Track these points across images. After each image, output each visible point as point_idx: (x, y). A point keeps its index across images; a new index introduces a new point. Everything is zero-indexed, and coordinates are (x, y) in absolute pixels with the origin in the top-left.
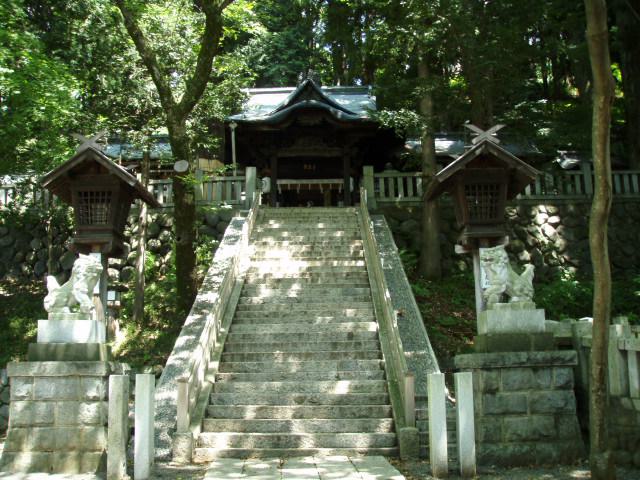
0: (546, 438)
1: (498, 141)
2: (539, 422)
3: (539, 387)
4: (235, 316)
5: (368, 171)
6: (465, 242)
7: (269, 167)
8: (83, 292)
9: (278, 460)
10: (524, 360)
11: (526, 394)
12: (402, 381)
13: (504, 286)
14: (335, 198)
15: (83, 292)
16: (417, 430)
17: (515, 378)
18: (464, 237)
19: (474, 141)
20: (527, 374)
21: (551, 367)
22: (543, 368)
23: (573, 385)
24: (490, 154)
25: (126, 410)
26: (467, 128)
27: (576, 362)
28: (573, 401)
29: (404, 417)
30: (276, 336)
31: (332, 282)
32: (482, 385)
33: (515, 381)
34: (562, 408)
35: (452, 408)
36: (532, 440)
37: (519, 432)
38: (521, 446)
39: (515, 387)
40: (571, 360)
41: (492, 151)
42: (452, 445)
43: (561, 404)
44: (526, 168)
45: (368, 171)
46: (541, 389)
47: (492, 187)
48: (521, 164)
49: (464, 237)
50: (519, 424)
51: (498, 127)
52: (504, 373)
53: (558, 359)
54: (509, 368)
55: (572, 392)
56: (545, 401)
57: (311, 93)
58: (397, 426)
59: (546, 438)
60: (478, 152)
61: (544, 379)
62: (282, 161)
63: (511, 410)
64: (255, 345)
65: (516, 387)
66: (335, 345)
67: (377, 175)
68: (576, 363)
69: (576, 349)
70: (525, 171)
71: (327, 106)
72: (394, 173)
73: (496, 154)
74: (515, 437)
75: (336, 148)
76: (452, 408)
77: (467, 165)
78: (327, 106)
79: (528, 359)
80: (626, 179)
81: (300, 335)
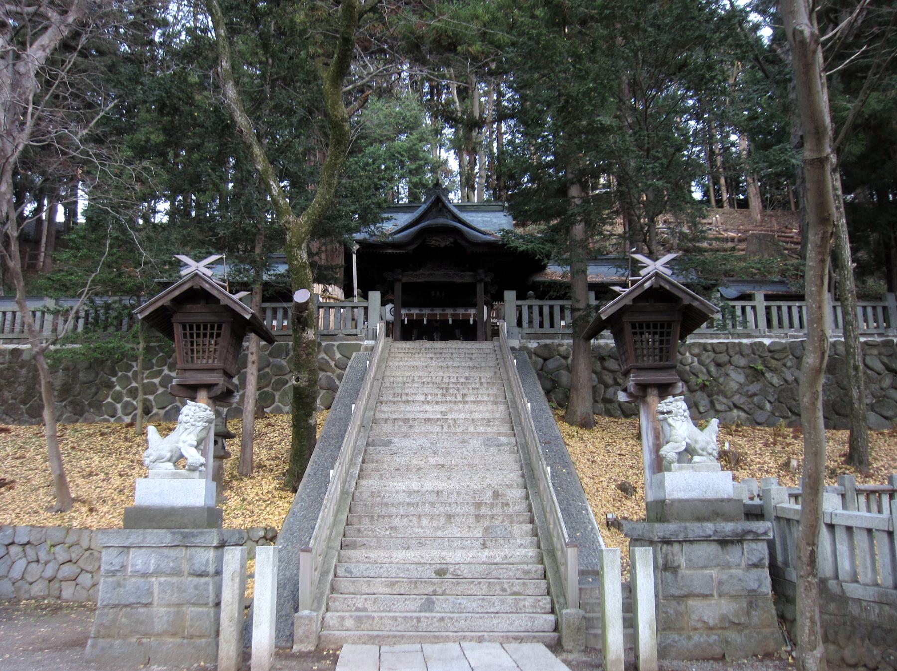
0: (737, 626)
1: (669, 272)
2: (727, 607)
3: (728, 566)
4: (361, 470)
5: (510, 296)
6: (632, 389)
7: (393, 293)
8: (191, 446)
9: (50, 303)
10: (711, 533)
11: (714, 572)
12: (564, 554)
13: (684, 444)
14: (467, 331)
15: (191, 446)
16: (581, 612)
17: (700, 553)
18: (631, 382)
19: (643, 272)
20: (713, 549)
21: (740, 542)
22: (732, 542)
23: (767, 562)
24: (661, 287)
25: (243, 588)
26: (633, 258)
27: (771, 535)
28: (768, 582)
29: (564, 596)
30: (410, 493)
31: (471, 429)
32: (661, 562)
33: (699, 557)
34: (755, 591)
35: (629, 590)
36: (721, 628)
37: (705, 619)
38: (708, 636)
39: (700, 565)
40: (766, 533)
41: (663, 284)
42: (631, 631)
43: (755, 586)
44: (702, 303)
45: (510, 296)
46: (730, 568)
47: (662, 327)
48: (697, 300)
49: (631, 382)
50: (708, 611)
51: (669, 257)
52: (686, 547)
53: (750, 531)
54: (691, 542)
55: (767, 572)
56: (735, 581)
57: (440, 210)
58: (557, 606)
59: (737, 626)
60: (647, 285)
61: (733, 555)
62: (406, 288)
63: (696, 592)
64: (386, 504)
65: (700, 565)
66: (478, 505)
67: (520, 303)
68: (772, 537)
69: (769, 520)
70: (701, 308)
71: (459, 225)
72: (536, 303)
73: (667, 287)
74: (699, 625)
75: (469, 273)
76: (629, 590)
77: (634, 300)
78: (459, 225)
79: (715, 531)
80: (795, 311)
81: (437, 493)
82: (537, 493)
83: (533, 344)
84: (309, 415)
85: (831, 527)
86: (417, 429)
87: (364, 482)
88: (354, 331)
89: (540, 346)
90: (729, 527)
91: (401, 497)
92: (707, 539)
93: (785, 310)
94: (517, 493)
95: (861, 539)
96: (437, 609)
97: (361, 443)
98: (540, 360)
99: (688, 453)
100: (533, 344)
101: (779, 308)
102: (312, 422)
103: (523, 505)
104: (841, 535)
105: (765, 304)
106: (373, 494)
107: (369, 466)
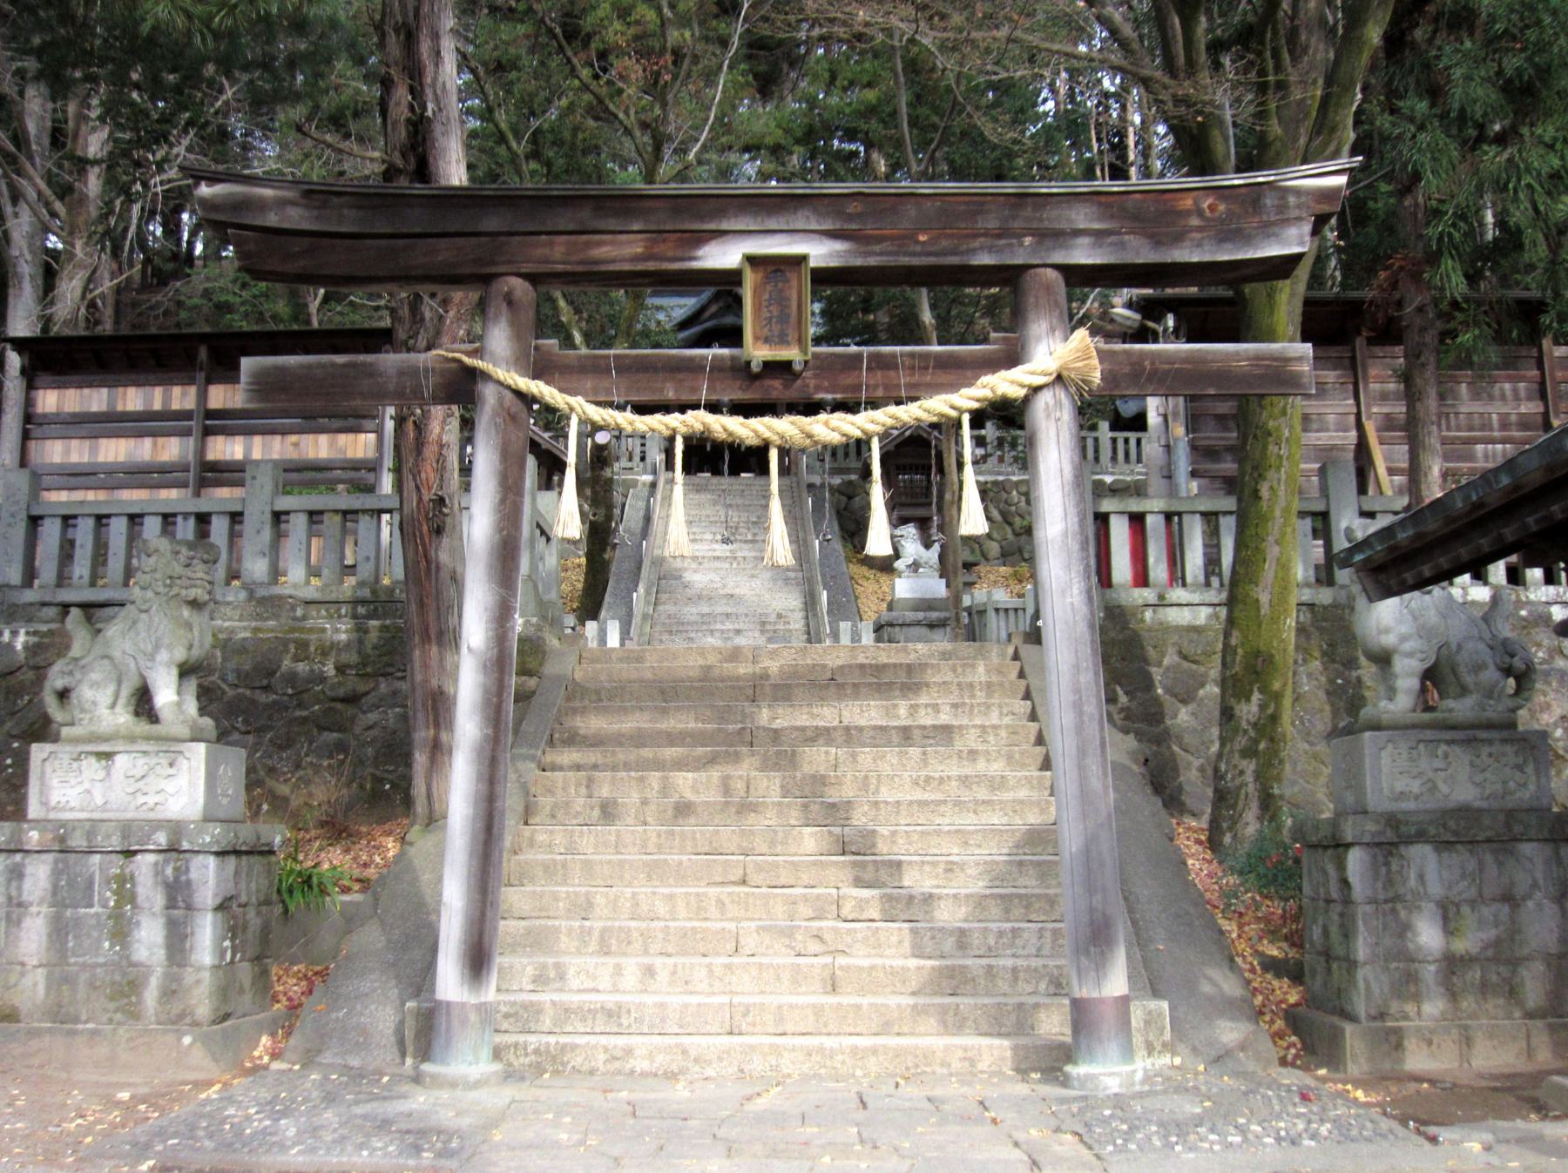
20: (924, 630)
82: (815, 615)
83: (837, 481)
84: (604, 550)
85: (997, 610)
86: (706, 565)
87: (661, 608)
88: (629, 465)
89: (844, 483)
90: (934, 615)
91: (693, 618)
92: (918, 624)
93: (1133, 443)
94: (799, 615)
95: (1011, 614)
96: (574, 983)
97: (654, 577)
98: (844, 499)
99: (915, 566)
100: (837, 481)
101: (1126, 441)
102: (606, 556)
103: (802, 622)
104: (1011, 614)
105: (1110, 434)
106: (669, 617)
107: (664, 597)
